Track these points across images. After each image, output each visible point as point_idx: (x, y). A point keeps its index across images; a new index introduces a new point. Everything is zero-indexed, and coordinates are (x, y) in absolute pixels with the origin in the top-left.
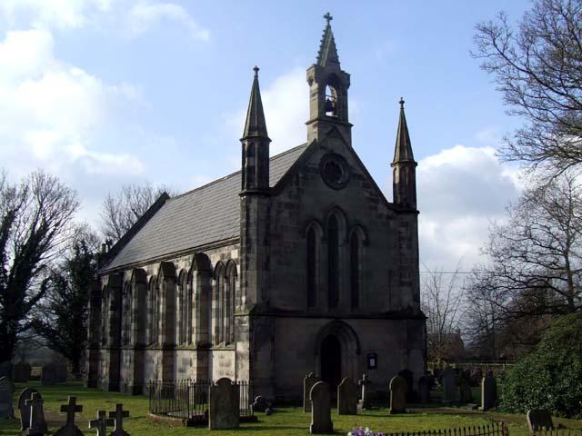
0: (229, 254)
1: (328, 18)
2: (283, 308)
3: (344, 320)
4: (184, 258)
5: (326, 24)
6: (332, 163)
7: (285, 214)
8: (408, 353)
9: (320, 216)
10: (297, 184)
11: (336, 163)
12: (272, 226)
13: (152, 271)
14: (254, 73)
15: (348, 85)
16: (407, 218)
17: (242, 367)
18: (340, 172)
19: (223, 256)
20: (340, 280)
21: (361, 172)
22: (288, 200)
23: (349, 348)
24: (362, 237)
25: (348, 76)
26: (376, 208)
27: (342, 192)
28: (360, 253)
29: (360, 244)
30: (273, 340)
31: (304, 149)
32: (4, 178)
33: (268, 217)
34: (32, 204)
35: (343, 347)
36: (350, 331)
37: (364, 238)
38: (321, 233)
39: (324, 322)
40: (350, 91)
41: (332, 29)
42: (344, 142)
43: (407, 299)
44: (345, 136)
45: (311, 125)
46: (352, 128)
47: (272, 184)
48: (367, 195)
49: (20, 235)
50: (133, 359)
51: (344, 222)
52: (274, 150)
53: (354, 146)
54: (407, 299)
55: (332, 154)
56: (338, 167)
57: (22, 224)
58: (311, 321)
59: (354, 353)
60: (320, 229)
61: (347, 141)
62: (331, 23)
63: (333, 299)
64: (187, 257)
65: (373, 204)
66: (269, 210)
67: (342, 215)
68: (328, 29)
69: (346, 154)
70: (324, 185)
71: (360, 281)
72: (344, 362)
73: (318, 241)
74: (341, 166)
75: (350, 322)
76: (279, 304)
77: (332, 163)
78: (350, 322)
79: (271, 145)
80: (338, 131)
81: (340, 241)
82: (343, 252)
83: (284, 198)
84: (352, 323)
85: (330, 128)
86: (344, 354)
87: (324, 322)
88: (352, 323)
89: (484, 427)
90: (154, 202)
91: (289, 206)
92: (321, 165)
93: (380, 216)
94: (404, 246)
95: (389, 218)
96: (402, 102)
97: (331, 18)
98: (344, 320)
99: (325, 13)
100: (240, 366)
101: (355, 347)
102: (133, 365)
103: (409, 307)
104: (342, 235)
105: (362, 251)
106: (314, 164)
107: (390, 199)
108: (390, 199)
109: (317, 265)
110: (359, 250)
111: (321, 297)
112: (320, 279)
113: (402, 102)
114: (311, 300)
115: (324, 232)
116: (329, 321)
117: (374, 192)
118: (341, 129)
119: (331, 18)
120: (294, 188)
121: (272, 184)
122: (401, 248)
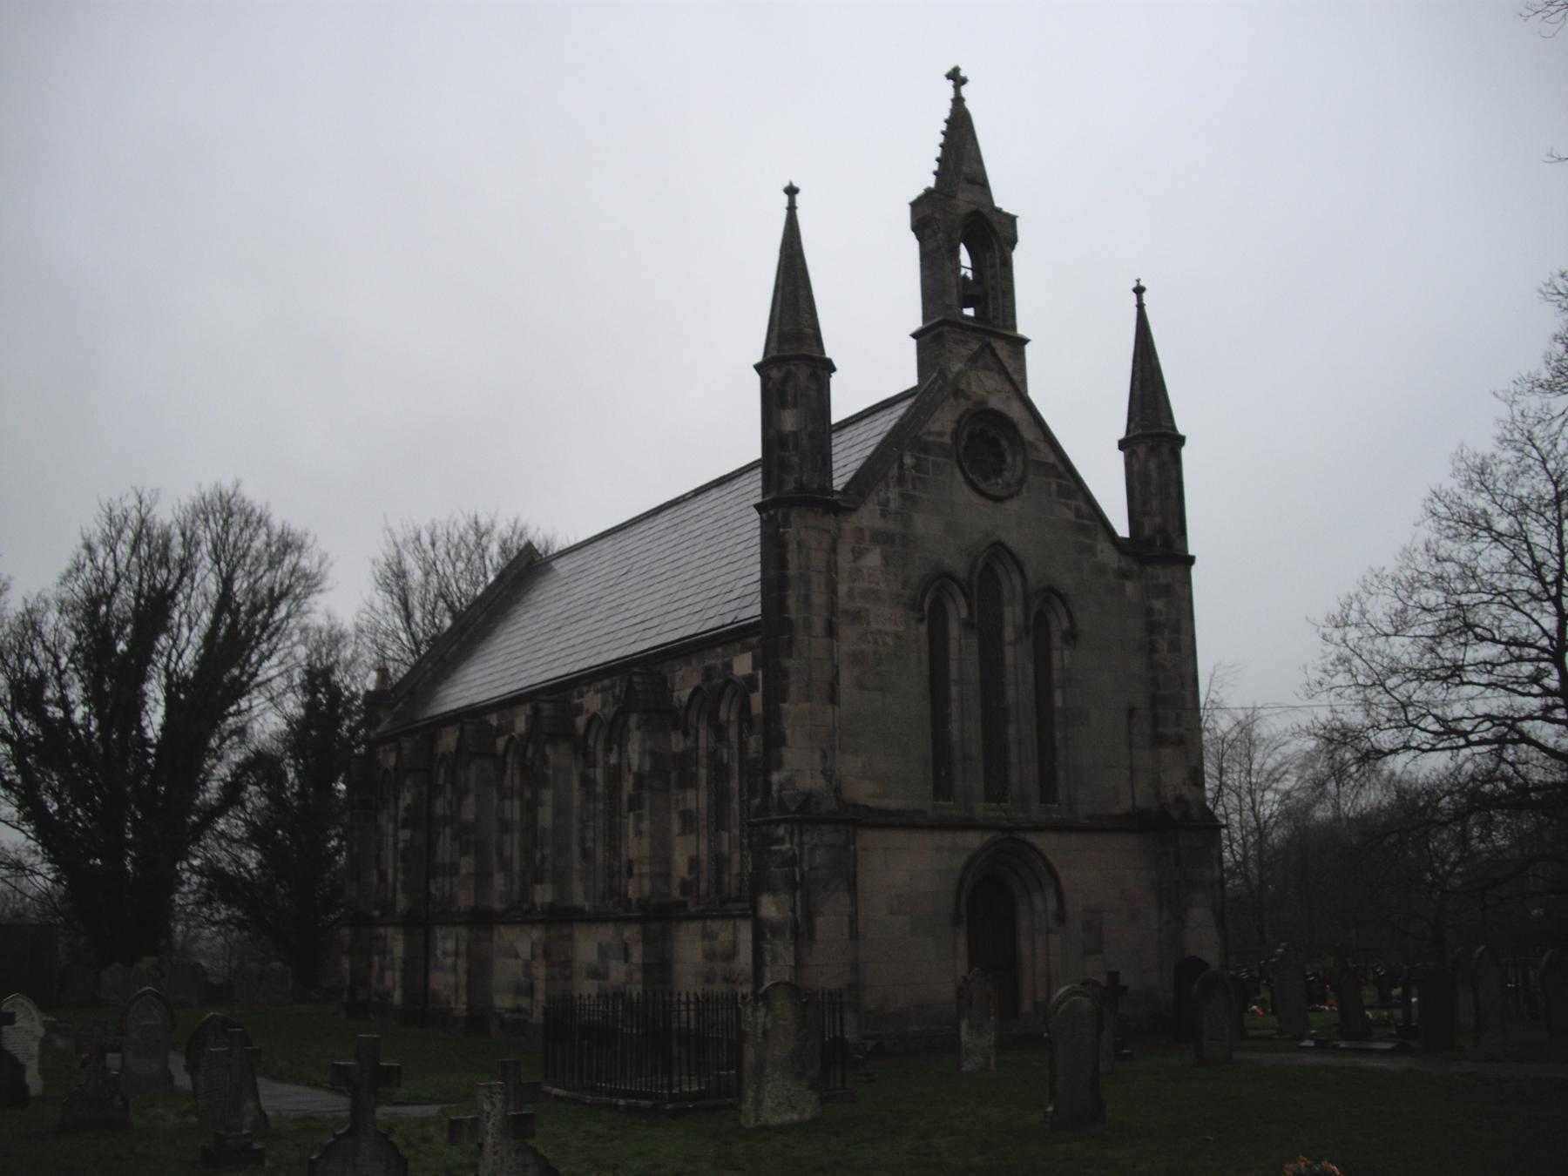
0: (728, 666)
1: (956, 78)
2: (873, 803)
3: (1021, 835)
4: (599, 685)
5: (951, 93)
7: (874, 559)
9: (958, 565)
10: (901, 480)
12: (843, 589)
13: (511, 726)
14: (785, 198)
15: (1012, 241)
16: (1163, 575)
17: (775, 959)
19: (708, 673)
21: (1052, 459)
22: (878, 523)
24: (1059, 623)
25: (1011, 220)
26: (1090, 550)
27: (1012, 505)
28: (1056, 663)
29: (1056, 641)
30: (853, 886)
31: (900, 410)
32: (140, 497)
34: (207, 581)
37: (1065, 624)
38: (964, 613)
39: (974, 840)
40: (1019, 257)
41: (968, 105)
42: (1010, 380)
43: (1174, 778)
44: (1010, 365)
45: (929, 336)
46: (1028, 347)
47: (839, 483)
48: (1070, 515)
49: (180, 656)
50: (463, 947)
52: (845, 399)
53: (1035, 392)
54: (1174, 778)
57: (185, 631)
58: (947, 839)
60: (962, 601)
61: (1016, 378)
62: (964, 90)
64: (607, 682)
65: (1086, 541)
66: (833, 550)
68: (958, 101)
69: (1014, 411)
70: (966, 489)
73: (954, 630)
74: (1004, 443)
76: (863, 792)
79: (835, 381)
80: (995, 355)
81: (1009, 634)
82: (1015, 657)
83: (868, 516)
84: (1045, 842)
85: (975, 346)
87: (974, 840)
90: (491, 578)
91: (880, 538)
92: (955, 435)
93: (1100, 570)
94: (1162, 645)
95: (1123, 574)
96: (1139, 291)
97: (964, 81)
98: (1021, 835)
99: (949, 69)
100: (768, 958)
101: (1052, 904)
102: (463, 965)
103: (1180, 800)
104: (1012, 615)
105: (1061, 658)
106: (941, 434)
107: (1122, 528)
108: (1122, 528)
110: (1056, 655)
112: (965, 728)
114: (942, 788)
115: (969, 606)
116: (988, 836)
117: (1084, 508)
118: (1002, 350)
119: (964, 81)
120: (893, 493)
121: (839, 483)
122: (1153, 649)
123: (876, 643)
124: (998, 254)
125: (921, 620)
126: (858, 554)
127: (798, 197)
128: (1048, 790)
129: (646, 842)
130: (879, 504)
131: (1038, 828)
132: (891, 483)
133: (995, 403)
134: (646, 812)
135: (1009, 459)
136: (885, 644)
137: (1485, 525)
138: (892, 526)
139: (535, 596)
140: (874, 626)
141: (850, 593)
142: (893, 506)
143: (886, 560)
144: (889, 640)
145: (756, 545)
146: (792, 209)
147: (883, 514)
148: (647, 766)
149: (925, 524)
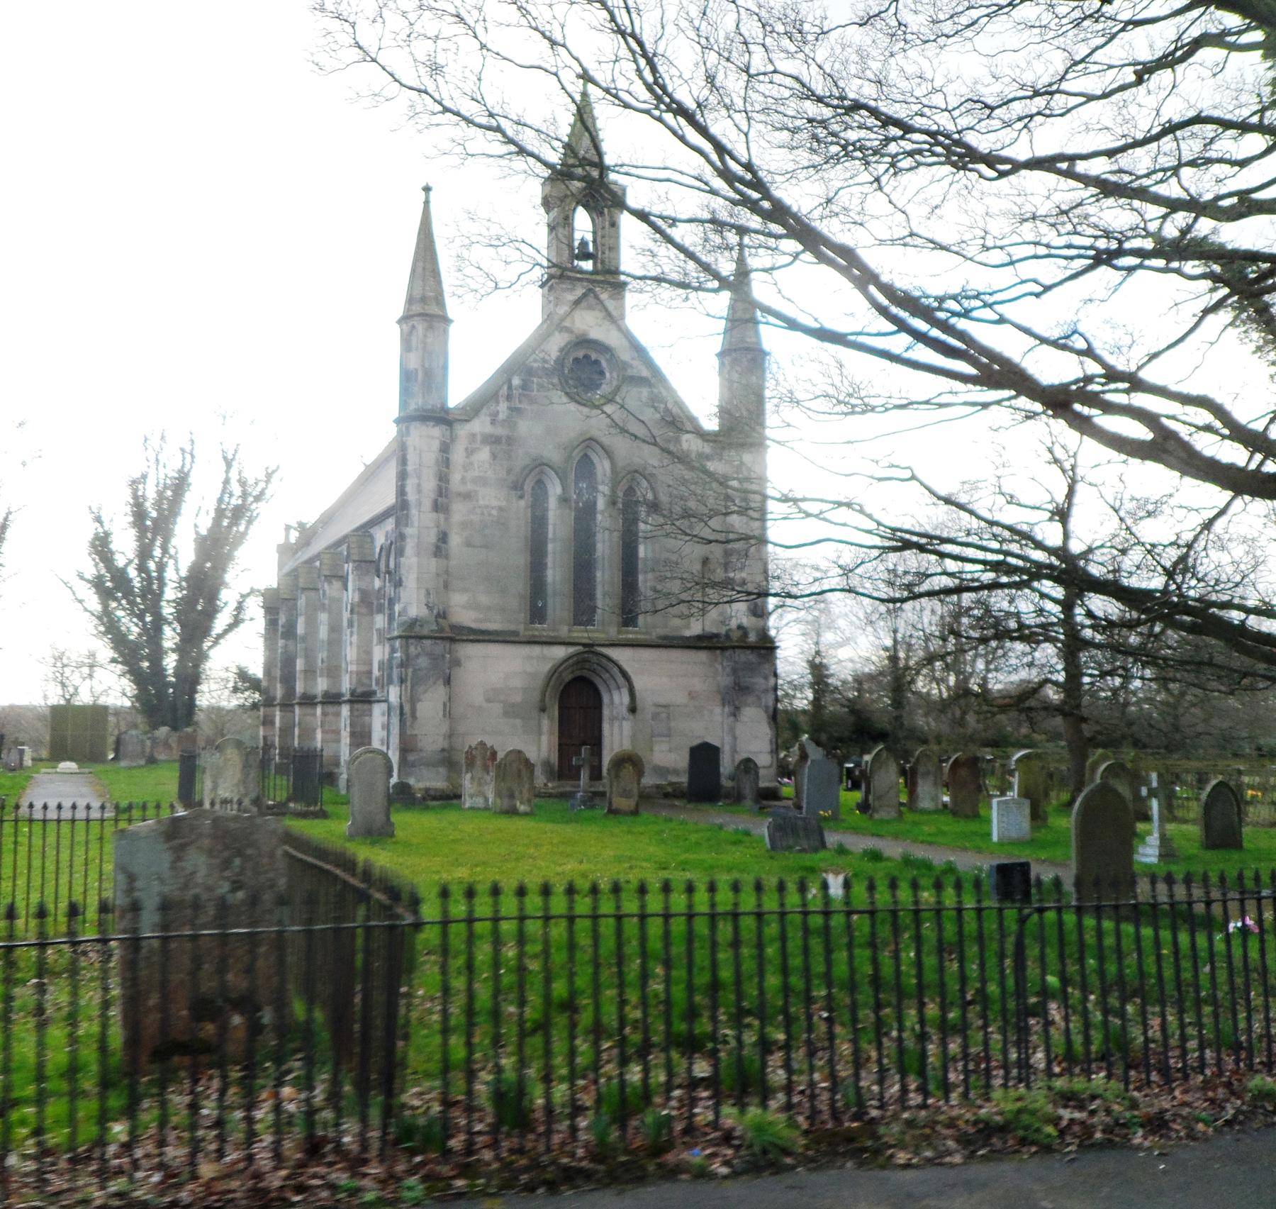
2: (474, 625)
6: (586, 357)
7: (484, 454)
8: (735, 713)
9: (556, 457)
11: (594, 356)
18: (602, 373)
20: (599, 574)
21: (645, 373)
22: (489, 429)
23: (615, 702)
30: (448, 681)
33: (447, 463)
35: (606, 699)
36: (616, 670)
39: (560, 652)
51: (607, 464)
55: (584, 342)
56: (597, 362)
58: (536, 650)
59: (624, 710)
60: (557, 482)
63: (583, 610)
67: (601, 452)
71: (641, 578)
72: (606, 727)
73: (552, 503)
74: (604, 363)
75: (614, 653)
76: (465, 617)
77: (586, 357)
78: (614, 653)
83: (480, 425)
84: (621, 656)
86: (606, 712)
87: (560, 652)
88: (621, 656)
89: (781, 887)
91: (493, 440)
96: (427, 189)
101: (626, 700)
109: (550, 547)
111: (558, 606)
113: (427, 189)
114: (537, 614)
116: (571, 650)
123: (483, 514)
124: (607, 217)
125: (521, 497)
126: (470, 452)
127: (431, 193)
128: (628, 616)
129: (355, 650)
130: (490, 415)
131: (613, 645)
132: (501, 399)
133: (595, 334)
134: (355, 629)
135: (608, 375)
136: (490, 515)
137: (390, 524)
138: (500, 431)
139: (474, 395)
140: (481, 502)
141: (463, 481)
142: (501, 416)
143: (494, 456)
144: (494, 512)
145: (1186, 190)
146: (427, 203)
147: (493, 422)
148: (356, 599)
149: (525, 427)
